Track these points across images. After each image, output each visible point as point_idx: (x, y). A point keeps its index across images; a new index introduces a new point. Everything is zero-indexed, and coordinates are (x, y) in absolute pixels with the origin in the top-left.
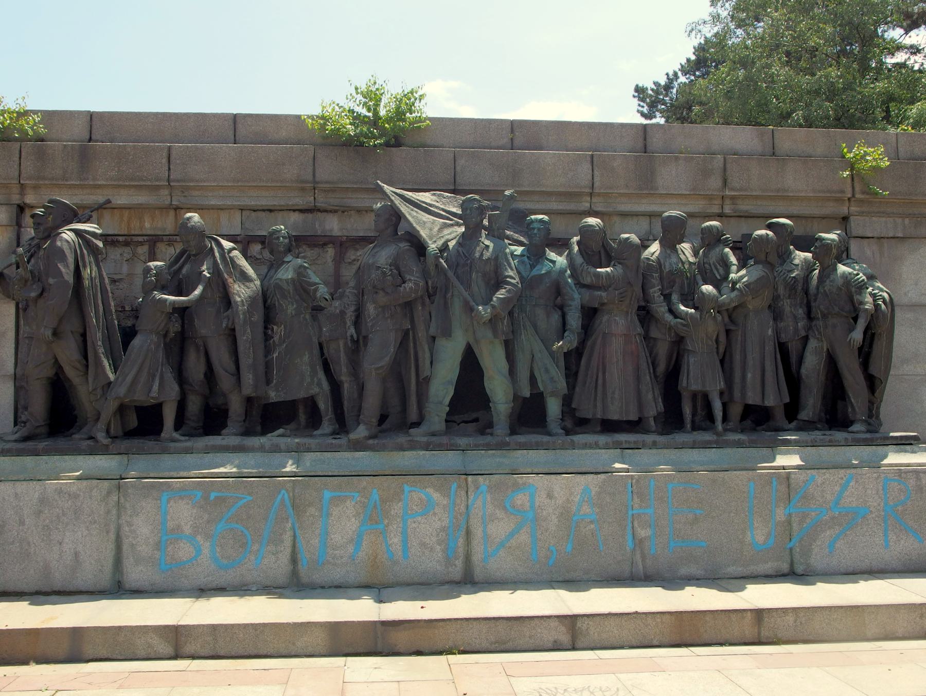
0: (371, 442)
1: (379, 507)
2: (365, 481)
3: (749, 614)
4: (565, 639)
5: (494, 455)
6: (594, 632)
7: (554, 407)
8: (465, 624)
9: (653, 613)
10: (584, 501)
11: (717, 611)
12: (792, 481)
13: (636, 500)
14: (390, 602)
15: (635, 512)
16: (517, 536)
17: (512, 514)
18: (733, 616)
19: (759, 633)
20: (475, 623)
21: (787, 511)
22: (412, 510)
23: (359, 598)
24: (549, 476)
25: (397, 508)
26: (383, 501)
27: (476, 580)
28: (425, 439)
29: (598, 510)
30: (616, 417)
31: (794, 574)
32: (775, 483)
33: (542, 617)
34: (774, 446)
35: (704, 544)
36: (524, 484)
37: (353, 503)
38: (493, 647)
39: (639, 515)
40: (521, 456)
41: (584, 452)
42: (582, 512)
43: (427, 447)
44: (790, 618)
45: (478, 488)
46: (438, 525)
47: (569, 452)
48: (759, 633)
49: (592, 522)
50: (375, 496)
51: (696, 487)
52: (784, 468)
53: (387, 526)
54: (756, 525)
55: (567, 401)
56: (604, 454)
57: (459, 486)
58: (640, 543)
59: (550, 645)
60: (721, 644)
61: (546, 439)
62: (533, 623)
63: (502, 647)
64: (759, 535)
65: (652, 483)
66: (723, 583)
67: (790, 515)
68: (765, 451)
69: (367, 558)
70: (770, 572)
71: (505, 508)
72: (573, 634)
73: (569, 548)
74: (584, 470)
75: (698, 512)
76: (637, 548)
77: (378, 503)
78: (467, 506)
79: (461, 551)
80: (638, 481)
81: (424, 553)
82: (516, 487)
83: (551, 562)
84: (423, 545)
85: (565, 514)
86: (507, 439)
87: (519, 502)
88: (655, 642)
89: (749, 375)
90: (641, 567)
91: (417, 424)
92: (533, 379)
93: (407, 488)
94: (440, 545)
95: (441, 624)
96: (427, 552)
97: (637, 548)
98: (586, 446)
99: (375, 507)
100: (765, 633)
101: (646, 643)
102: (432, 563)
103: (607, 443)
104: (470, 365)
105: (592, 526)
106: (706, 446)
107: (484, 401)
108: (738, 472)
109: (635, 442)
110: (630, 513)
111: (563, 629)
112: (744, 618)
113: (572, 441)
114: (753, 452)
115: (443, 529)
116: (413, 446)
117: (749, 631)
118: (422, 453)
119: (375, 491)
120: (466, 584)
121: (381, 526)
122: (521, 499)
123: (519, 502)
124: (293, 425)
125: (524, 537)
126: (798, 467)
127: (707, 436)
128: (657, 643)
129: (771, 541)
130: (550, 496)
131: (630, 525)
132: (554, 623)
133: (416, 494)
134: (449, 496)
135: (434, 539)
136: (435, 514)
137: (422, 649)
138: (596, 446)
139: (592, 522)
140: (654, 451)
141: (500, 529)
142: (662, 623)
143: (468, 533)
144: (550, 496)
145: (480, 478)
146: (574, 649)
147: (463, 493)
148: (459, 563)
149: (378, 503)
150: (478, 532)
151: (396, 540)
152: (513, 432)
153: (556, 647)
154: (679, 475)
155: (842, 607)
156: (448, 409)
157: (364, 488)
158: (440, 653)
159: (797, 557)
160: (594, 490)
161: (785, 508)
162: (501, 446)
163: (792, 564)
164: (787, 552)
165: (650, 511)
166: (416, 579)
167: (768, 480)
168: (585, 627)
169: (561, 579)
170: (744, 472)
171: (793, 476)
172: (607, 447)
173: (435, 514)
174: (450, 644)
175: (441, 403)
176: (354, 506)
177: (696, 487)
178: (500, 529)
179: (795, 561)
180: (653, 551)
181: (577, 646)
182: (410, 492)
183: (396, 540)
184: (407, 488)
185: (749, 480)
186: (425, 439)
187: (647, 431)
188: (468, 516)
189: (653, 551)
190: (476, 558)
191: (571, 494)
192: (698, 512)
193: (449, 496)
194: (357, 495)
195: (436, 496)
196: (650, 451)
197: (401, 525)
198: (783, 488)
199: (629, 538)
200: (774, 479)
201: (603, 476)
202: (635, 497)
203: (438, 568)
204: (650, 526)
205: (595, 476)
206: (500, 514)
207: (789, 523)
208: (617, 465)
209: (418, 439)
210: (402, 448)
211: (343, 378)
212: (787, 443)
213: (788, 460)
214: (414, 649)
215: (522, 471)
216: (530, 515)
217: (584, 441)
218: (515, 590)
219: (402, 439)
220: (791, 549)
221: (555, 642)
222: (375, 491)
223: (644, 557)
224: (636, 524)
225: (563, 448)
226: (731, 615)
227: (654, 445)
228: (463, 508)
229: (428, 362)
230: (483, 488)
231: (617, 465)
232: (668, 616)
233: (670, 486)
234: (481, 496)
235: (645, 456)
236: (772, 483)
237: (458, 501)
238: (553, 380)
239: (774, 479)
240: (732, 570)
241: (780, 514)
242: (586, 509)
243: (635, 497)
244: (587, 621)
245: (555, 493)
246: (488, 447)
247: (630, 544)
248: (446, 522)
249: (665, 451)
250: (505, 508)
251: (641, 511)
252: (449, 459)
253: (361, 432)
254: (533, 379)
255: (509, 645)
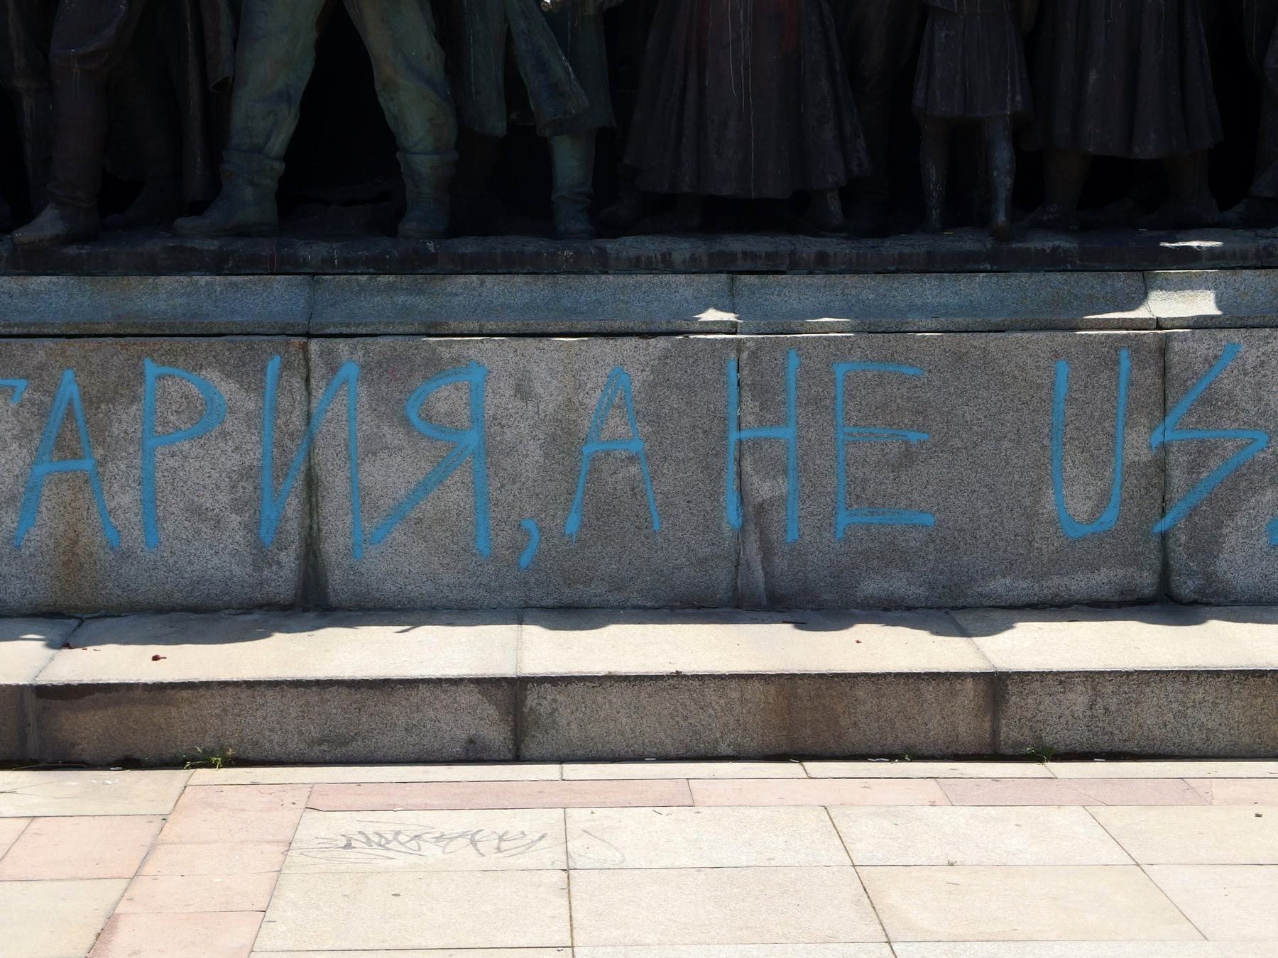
0: (71, 251)
1: (79, 415)
2: (41, 350)
3: (969, 684)
4: (495, 733)
5: (390, 286)
6: (569, 718)
7: (570, 163)
8: (245, 694)
9: (722, 677)
10: (611, 405)
11: (885, 675)
12: (1173, 359)
13: (750, 404)
14: (83, 645)
15: (745, 434)
16: (436, 492)
17: (423, 436)
18: (928, 691)
19: (995, 733)
20: (270, 693)
21: (1157, 439)
22: (166, 423)
23: (15, 637)
24: (521, 341)
25: (125, 420)
26: (91, 401)
27: (333, 599)
28: (213, 245)
29: (648, 429)
30: (728, 190)
31: (1168, 602)
32: (1125, 364)
33: (438, 682)
34: (1149, 266)
35: (928, 520)
36: (456, 360)
37: (13, 405)
38: (316, 751)
39: (757, 444)
40: (463, 289)
41: (630, 280)
42: (606, 435)
43: (217, 266)
44: (1079, 699)
45: (334, 370)
46: (233, 461)
47: (591, 280)
48: (995, 733)
49: (632, 459)
50: (70, 386)
51: (908, 371)
52: (1158, 324)
53: (102, 463)
54: (1070, 472)
55: (607, 150)
56: (682, 286)
57: (286, 366)
58: (757, 513)
59: (458, 750)
60: (892, 757)
61: (533, 245)
62: (415, 696)
63: (339, 752)
64: (1077, 499)
65: (793, 361)
66: (962, 618)
67: (1164, 447)
68: (1122, 281)
69: (51, 543)
70: (1105, 593)
71: (405, 422)
72: (517, 725)
73: (573, 525)
74: (616, 325)
75: (914, 437)
76: (751, 527)
77: (78, 405)
78: (308, 417)
79: (293, 528)
80: (753, 355)
81: (198, 532)
82: (435, 367)
83: (525, 560)
84: (196, 512)
85: (563, 439)
86: (431, 246)
87: (442, 407)
88: (724, 748)
89: (1093, 76)
90: (759, 574)
91: (197, 209)
92: (514, 91)
93: (151, 369)
94: (238, 511)
95: (184, 694)
96: (205, 529)
97: (751, 527)
98: (637, 266)
99: (70, 415)
100: (1010, 732)
101: (701, 748)
102: (221, 558)
103: (693, 258)
104: (341, 56)
105: (633, 470)
106: (961, 265)
107: (381, 141)
108: (1026, 335)
109: (769, 256)
110: (734, 436)
111: (491, 711)
112: (954, 694)
113: (602, 252)
114: (1088, 282)
115: (248, 473)
116: (182, 263)
117: (968, 727)
118: (203, 280)
119: (69, 374)
120: (306, 610)
121: (87, 465)
122: (446, 397)
123: (442, 407)
124: (197, 234)
125: (454, 495)
126: (1200, 324)
127: (968, 242)
128: (729, 751)
129: (1110, 516)
130: (523, 391)
131: (732, 468)
132: (469, 698)
133: (175, 383)
134: (260, 389)
135: (224, 498)
136: (225, 435)
137: (138, 755)
138: (666, 265)
139: (632, 459)
140: (819, 279)
141: (394, 473)
142: (743, 700)
143: (311, 484)
144: (523, 391)
145: (342, 346)
146: (518, 758)
147: (297, 383)
148: (289, 559)
149: (78, 405)
150: (336, 481)
151: (125, 499)
152: (455, 230)
153: (474, 754)
154: (863, 340)
155: (1217, 673)
156: (280, 167)
157: (42, 367)
158: (176, 763)
159: (1179, 555)
160: (639, 378)
161: (1152, 430)
162: (415, 264)
163: (1165, 573)
164: (1154, 544)
165: (786, 433)
166: (178, 598)
167: (1107, 357)
168: (544, 709)
169: (550, 602)
170: (1042, 335)
171: (1176, 346)
172: (693, 267)
173: (225, 435)
174: (209, 742)
175: (259, 150)
176: (16, 413)
177: (908, 371)
178: (394, 473)
179: (1175, 565)
180: (790, 537)
181: (525, 753)
182: (161, 377)
183: (125, 499)
184: (151, 369)
185: (1056, 355)
186: (213, 245)
187: (818, 229)
188: (311, 441)
189: (790, 537)
190: (333, 547)
191: (579, 387)
192: (914, 437)
193: (260, 389)
194: (21, 384)
195: (227, 389)
196: (808, 279)
197: (138, 462)
198: (1149, 376)
199: (730, 499)
200: (1124, 354)
201: (662, 343)
202: (747, 395)
203: (237, 570)
204: (785, 472)
205: (642, 343)
206: (393, 436)
207: (1162, 467)
208: (711, 315)
209: (197, 244)
210: (152, 268)
211: (20, 84)
212: (1190, 259)
213: (1179, 303)
214: (118, 754)
215: (454, 326)
216: (472, 439)
217: (633, 253)
218: (416, 624)
219: (154, 246)
220: (1164, 536)
221: (471, 741)
222: (69, 374)
223: (767, 551)
224: (748, 466)
225: (578, 269)
226: (923, 685)
227: (822, 264)
228: (297, 421)
229: (226, 42)
230: (350, 370)
231: (711, 315)
232: (756, 684)
233: (840, 370)
234: (344, 393)
235: (790, 291)
236: (1117, 362)
237: (285, 403)
238: (567, 91)
239: (1124, 354)
240: (1000, 586)
241: (1138, 444)
242: (617, 425)
243: (747, 395)
244: (550, 692)
245: (537, 384)
246: (379, 266)
247: (731, 517)
248: (253, 456)
249: (849, 279)
250: (405, 422)
251: (764, 433)
252: (276, 295)
253: (47, 224)
254: (514, 91)
255: (357, 747)
